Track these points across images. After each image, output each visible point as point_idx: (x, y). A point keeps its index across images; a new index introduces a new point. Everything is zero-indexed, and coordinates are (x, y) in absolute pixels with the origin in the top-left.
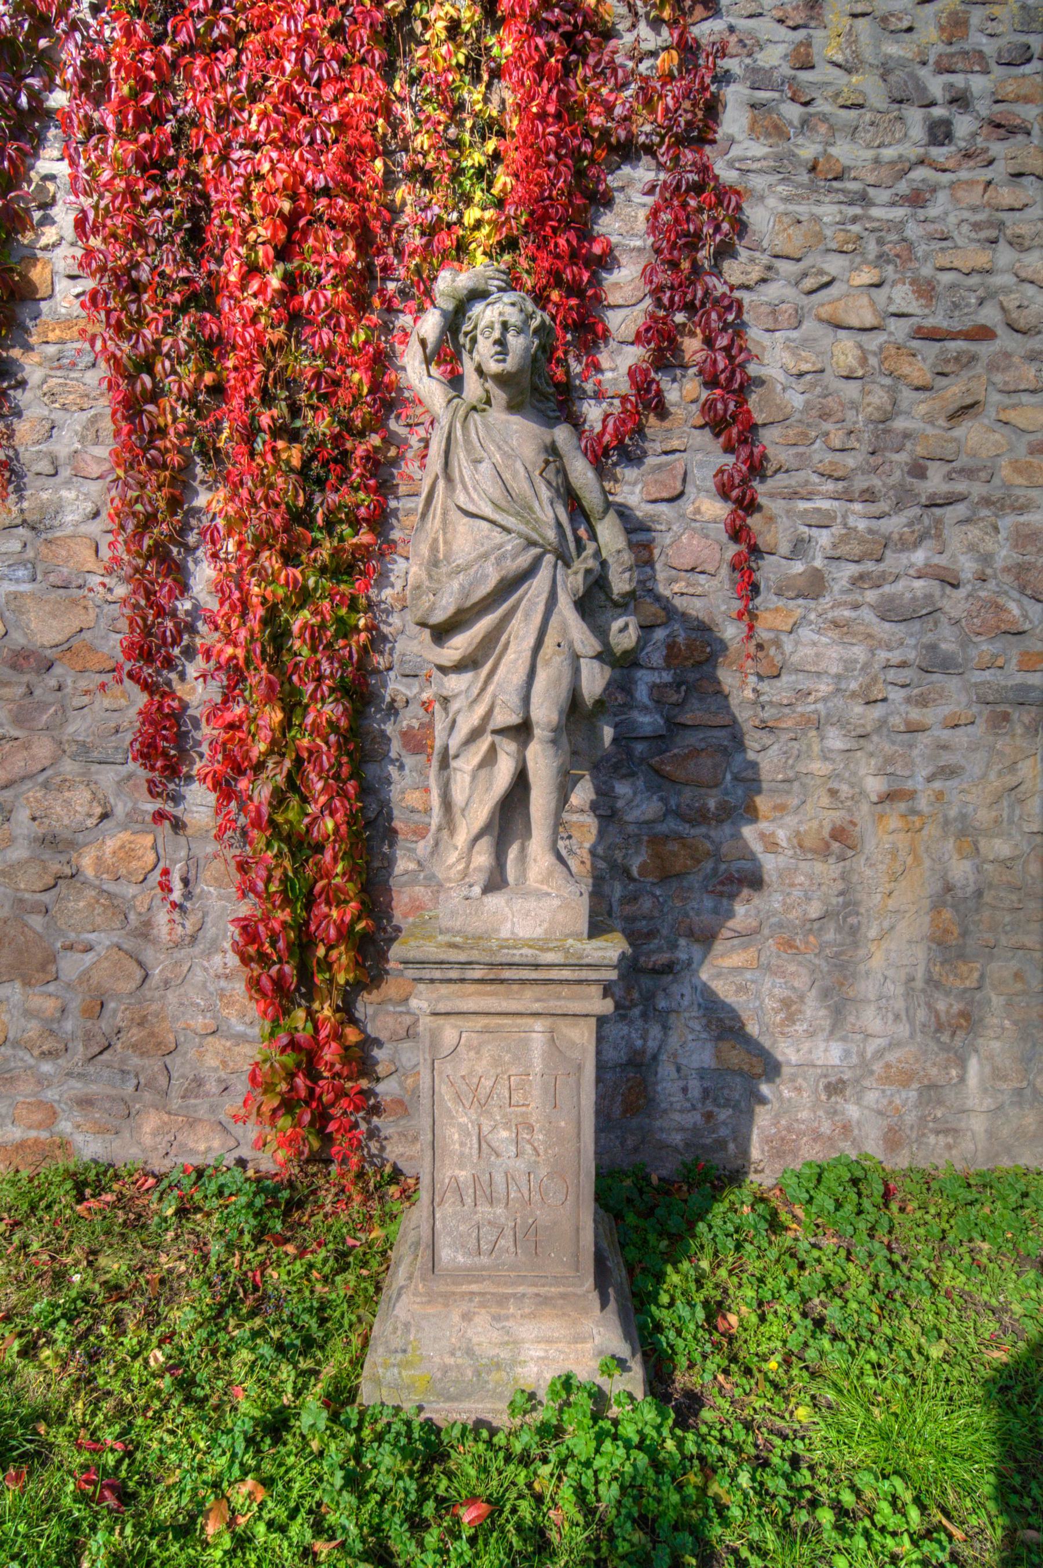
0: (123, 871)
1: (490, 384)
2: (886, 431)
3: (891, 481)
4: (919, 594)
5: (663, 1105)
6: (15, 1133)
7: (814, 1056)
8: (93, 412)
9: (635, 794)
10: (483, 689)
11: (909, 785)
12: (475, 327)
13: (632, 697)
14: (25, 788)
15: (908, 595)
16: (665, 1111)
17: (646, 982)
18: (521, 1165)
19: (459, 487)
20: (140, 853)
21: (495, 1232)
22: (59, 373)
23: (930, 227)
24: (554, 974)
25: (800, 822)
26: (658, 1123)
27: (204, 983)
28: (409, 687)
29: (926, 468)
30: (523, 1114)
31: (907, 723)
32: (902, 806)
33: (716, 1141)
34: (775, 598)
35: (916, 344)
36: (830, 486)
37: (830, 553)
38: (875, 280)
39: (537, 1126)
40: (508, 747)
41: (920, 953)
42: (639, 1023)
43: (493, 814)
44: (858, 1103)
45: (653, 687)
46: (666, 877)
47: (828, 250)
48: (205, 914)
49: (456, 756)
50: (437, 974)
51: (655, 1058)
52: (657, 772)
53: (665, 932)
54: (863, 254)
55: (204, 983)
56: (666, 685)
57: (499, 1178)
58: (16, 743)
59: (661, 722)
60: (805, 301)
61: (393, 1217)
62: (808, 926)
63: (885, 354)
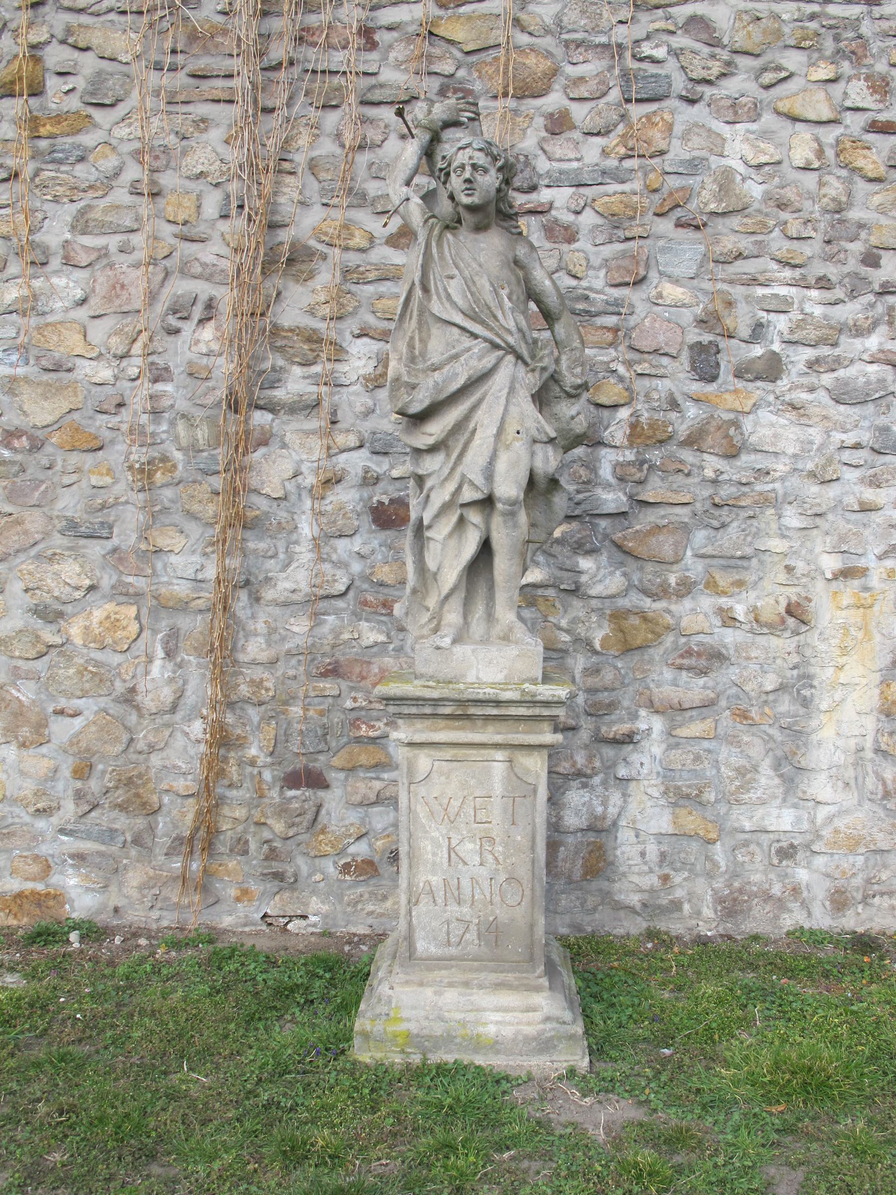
0: (109, 641)
1: (460, 209)
2: (841, 221)
3: (846, 269)
4: (873, 378)
5: (622, 869)
6: (14, 885)
7: (767, 822)
8: (82, 204)
9: (598, 569)
10: (453, 469)
11: (862, 563)
12: (449, 165)
13: (596, 474)
14: (18, 561)
15: (862, 380)
16: (624, 874)
17: (609, 752)
18: (484, 872)
19: (435, 297)
20: (124, 623)
22: (50, 167)
23: (885, 25)
25: (758, 598)
26: (617, 885)
27: (185, 748)
28: (379, 464)
29: (879, 257)
31: (861, 503)
32: (856, 583)
33: (672, 902)
35: (871, 137)
36: (787, 273)
37: (787, 337)
38: (831, 76)
39: (498, 840)
40: (475, 517)
41: (870, 724)
42: (600, 789)
43: (460, 577)
44: (808, 866)
45: (617, 465)
46: (628, 649)
47: (787, 47)
48: (185, 683)
49: (429, 527)
50: (414, 710)
51: (615, 824)
52: (619, 547)
53: (626, 703)
54: (819, 50)
55: (185, 748)
56: (629, 463)
57: (465, 883)
58: (10, 519)
59: (625, 499)
61: (343, 1052)
62: (764, 697)
63: (841, 146)
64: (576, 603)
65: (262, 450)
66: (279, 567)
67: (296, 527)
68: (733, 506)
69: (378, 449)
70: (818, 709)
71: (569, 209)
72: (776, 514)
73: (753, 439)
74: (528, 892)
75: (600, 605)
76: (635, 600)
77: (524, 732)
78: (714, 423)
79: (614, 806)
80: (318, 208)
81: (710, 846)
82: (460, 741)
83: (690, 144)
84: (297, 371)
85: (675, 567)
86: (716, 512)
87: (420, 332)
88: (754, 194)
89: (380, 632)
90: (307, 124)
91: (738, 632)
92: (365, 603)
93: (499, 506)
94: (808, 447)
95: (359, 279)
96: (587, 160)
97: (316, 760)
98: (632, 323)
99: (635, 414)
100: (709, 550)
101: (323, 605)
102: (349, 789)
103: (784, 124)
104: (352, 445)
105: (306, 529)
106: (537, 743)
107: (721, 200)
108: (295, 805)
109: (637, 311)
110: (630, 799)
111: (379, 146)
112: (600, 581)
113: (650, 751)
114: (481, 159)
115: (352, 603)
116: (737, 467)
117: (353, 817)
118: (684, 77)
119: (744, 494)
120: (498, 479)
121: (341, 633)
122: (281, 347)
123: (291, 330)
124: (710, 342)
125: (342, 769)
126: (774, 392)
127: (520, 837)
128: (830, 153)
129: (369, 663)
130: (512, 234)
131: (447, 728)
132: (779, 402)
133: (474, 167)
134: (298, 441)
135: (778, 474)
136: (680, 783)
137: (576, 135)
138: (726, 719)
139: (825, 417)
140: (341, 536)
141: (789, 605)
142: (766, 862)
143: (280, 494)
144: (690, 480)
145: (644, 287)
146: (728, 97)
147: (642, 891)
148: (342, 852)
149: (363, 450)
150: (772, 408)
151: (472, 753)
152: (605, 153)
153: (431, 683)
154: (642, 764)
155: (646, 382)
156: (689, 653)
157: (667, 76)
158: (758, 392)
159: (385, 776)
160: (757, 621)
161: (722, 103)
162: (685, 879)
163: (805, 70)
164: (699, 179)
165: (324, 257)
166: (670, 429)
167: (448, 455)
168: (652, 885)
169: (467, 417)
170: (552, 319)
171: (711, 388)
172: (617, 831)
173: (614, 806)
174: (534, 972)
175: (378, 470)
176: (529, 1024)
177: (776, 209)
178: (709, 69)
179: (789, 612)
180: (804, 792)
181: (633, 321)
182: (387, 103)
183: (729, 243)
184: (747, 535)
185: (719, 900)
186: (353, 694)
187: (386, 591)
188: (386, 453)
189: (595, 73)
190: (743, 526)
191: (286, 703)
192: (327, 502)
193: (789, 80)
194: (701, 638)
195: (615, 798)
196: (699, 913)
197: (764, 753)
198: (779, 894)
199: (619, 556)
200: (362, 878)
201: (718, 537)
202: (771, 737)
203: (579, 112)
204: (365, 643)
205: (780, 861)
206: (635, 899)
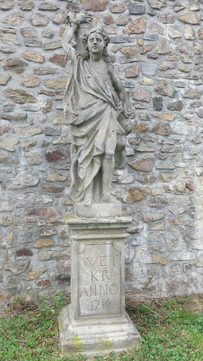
7: (182, 257)
9: (124, 174)
10: (90, 144)
12: (87, 38)
16: (136, 278)
21: (97, 303)
24: (113, 227)
25: (176, 182)
30: (104, 268)
34: (167, 110)
36: (184, 75)
37: (184, 96)
39: (108, 271)
43: (92, 181)
44: (196, 271)
49: (81, 164)
50: (79, 228)
51: (132, 261)
52: (131, 167)
60: (175, 14)
64: (117, 186)
65: (6, 134)
66: (13, 176)
67: (19, 162)
68: (168, 152)
69: (48, 134)
70: (197, 219)
71: (112, 51)
72: (182, 155)
73: (173, 130)
74: (119, 289)
75: (125, 187)
76: (137, 184)
77: (117, 234)
78: (161, 125)
79: (132, 255)
80: (24, 47)
81: (164, 267)
82: (96, 238)
83: (152, 30)
84: (18, 105)
85: (149, 173)
86: (163, 154)
87: (75, 96)
88: (173, 48)
89: (50, 198)
90: (19, 16)
91: (170, 194)
92: (44, 188)
93: (107, 156)
94: (191, 132)
95: (40, 73)
96: (118, 34)
97: (27, 245)
98: (134, 91)
99: (136, 122)
100: (160, 167)
101: (28, 190)
102: (40, 255)
103: (182, 24)
104: (39, 132)
105: (23, 162)
106: (122, 237)
107: (163, 49)
108: (20, 262)
109: (136, 86)
110: (137, 252)
111: (46, 26)
112: (125, 178)
113: (143, 235)
114: (100, 37)
115: (39, 188)
116: (169, 139)
117: (41, 265)
118: (150, 7)
119: (171, 148)
120: (107, 147)
121: (36, 199)
122: (12, 97)
123: (15, 91)
124: (160, 97)
125: (38, 248)
126: (180, 114)
127: (116, 270)
128: (197, 35)
129: (46, 209)
130: (106, 62)
131: (90, 233)
132: (181, 117)
133: (97, 39)
134: (19, 131)
135: (182, 141)
136: (153, 246)
137: (114, 25)
138: (168, 224)
139: (196, 122)
140: (35, 165)
141: (186, 184)
142: (182, 271)
143: (13, 150)
144: (154, 144)
145: (138, 78)
146: (164, 14)
147: (142, 284)
148: (38, 278)
149: (43, 134)
150: (179, 119)
151: (100, 242)
152: (124, 32)
153: (84, 218)
154: (141, 240)
155: (139, 111)
156: (154, 202)
157: (144, 6)
158: (175, 114)
159: (53, 249)
160: (177, 190)
161: (162, 16)
162: (156, 279)
163: (188, 6)
164: (155, 42)
165: (27, 65)
166: (147, 127)
167: (88, 139)
168: (145, 282)
169: (96, 126)
170: (119, 91)
171: (160, 113)
172: (133, 264)
173: (132, 255)
174: (122, 317)
175: (48, 141)
176: (123, 336)
177: (180, 53)
178: (158, 4)
179: (187, 187)
180: (193, 247)
181: (134, 90)
182: (48, 10)
183: (165, 64)
184: (172, 162)
185: (168, 285)
186: (41, 221)
187: (52, 184)
188: (51, 135)
189: (120, 4)
190: (171, 159)
191: (16, 225)
192: (30, 152)
193: (183, 10)
194: (159, 196)
195: (132, 252)
196: (161, 290)
197: (180, 234)
198: (187, 281)
199: (131, 169)
200: (45, 287)
201: (163, 163)
202: (182, 229)
203: (115, 17)
204: (45, 202)
205: (187, 270)
206: (140, 287)
